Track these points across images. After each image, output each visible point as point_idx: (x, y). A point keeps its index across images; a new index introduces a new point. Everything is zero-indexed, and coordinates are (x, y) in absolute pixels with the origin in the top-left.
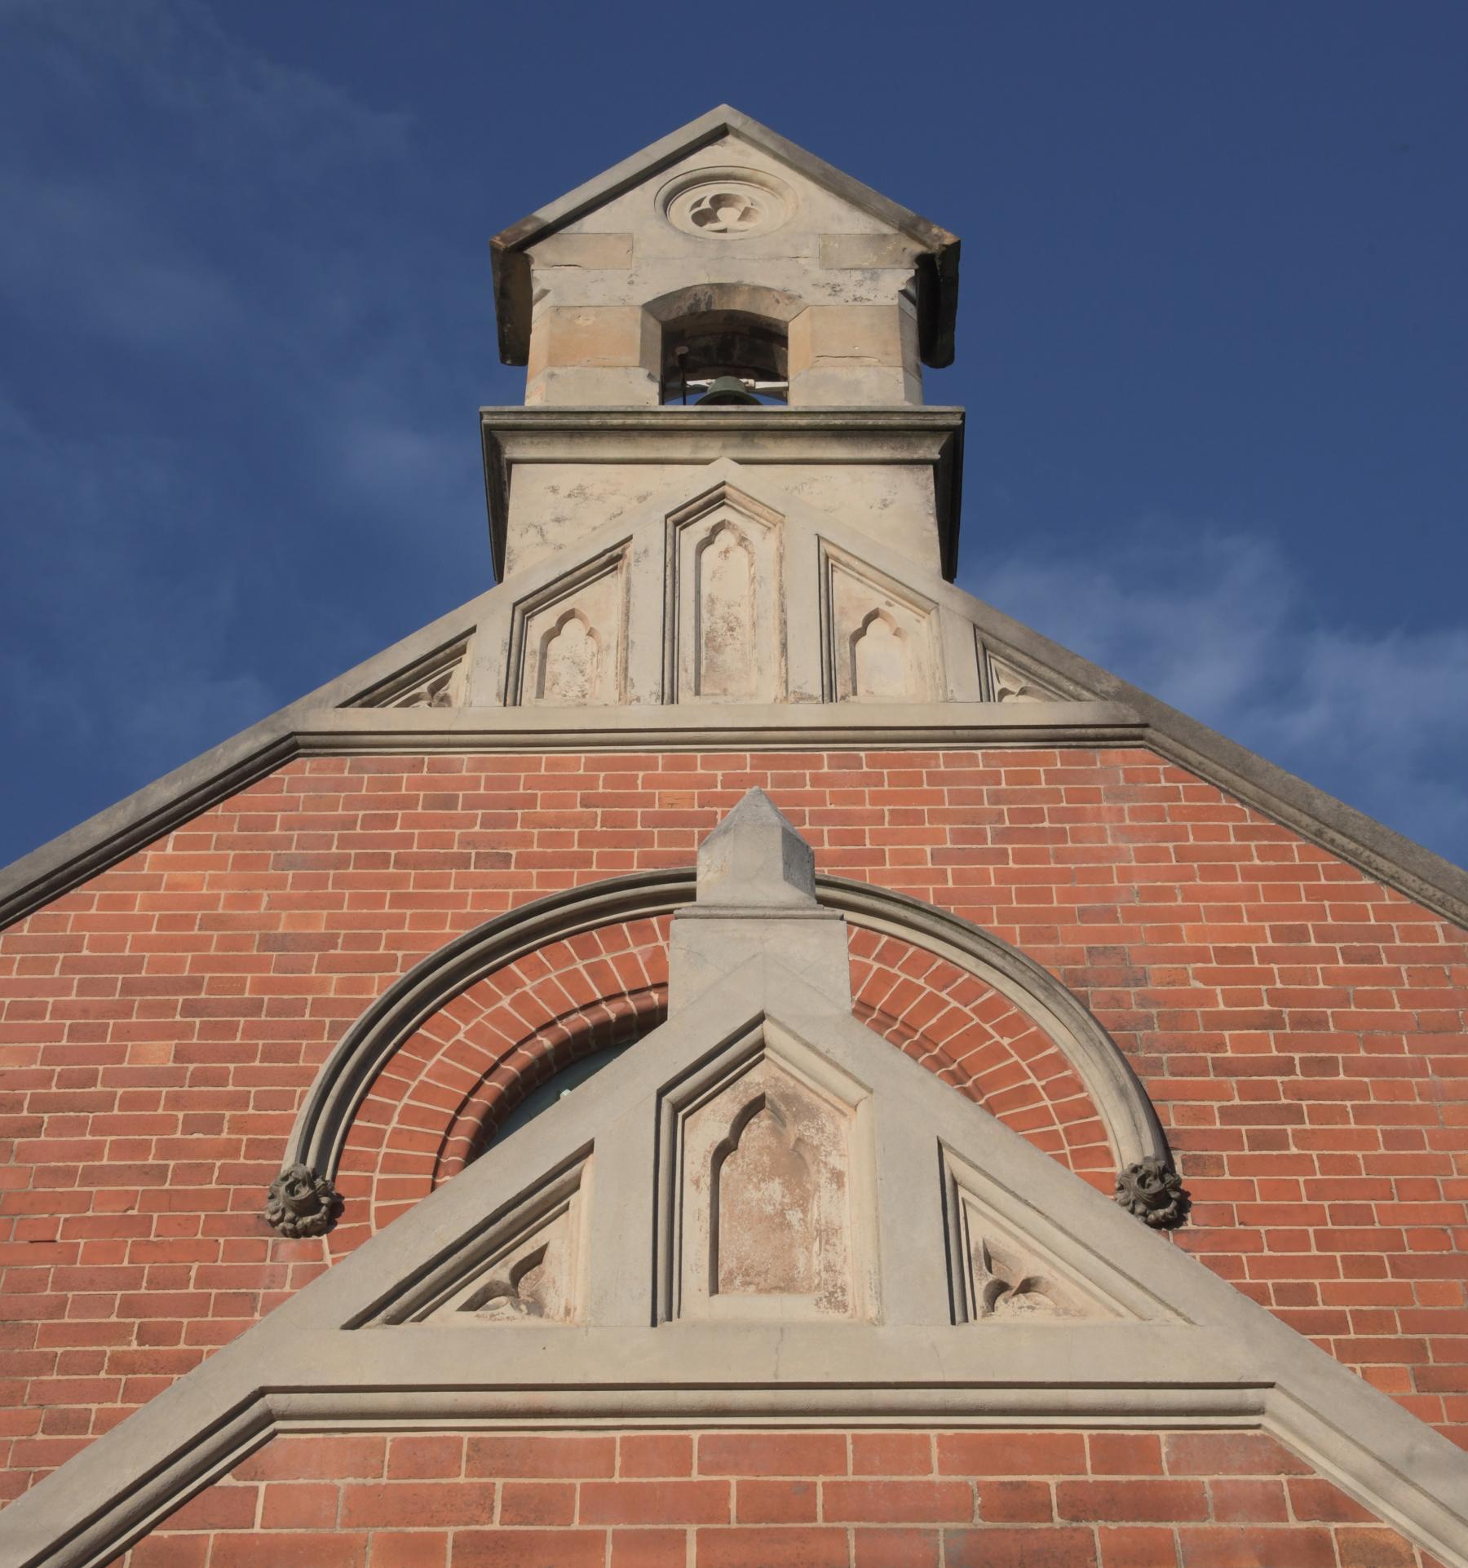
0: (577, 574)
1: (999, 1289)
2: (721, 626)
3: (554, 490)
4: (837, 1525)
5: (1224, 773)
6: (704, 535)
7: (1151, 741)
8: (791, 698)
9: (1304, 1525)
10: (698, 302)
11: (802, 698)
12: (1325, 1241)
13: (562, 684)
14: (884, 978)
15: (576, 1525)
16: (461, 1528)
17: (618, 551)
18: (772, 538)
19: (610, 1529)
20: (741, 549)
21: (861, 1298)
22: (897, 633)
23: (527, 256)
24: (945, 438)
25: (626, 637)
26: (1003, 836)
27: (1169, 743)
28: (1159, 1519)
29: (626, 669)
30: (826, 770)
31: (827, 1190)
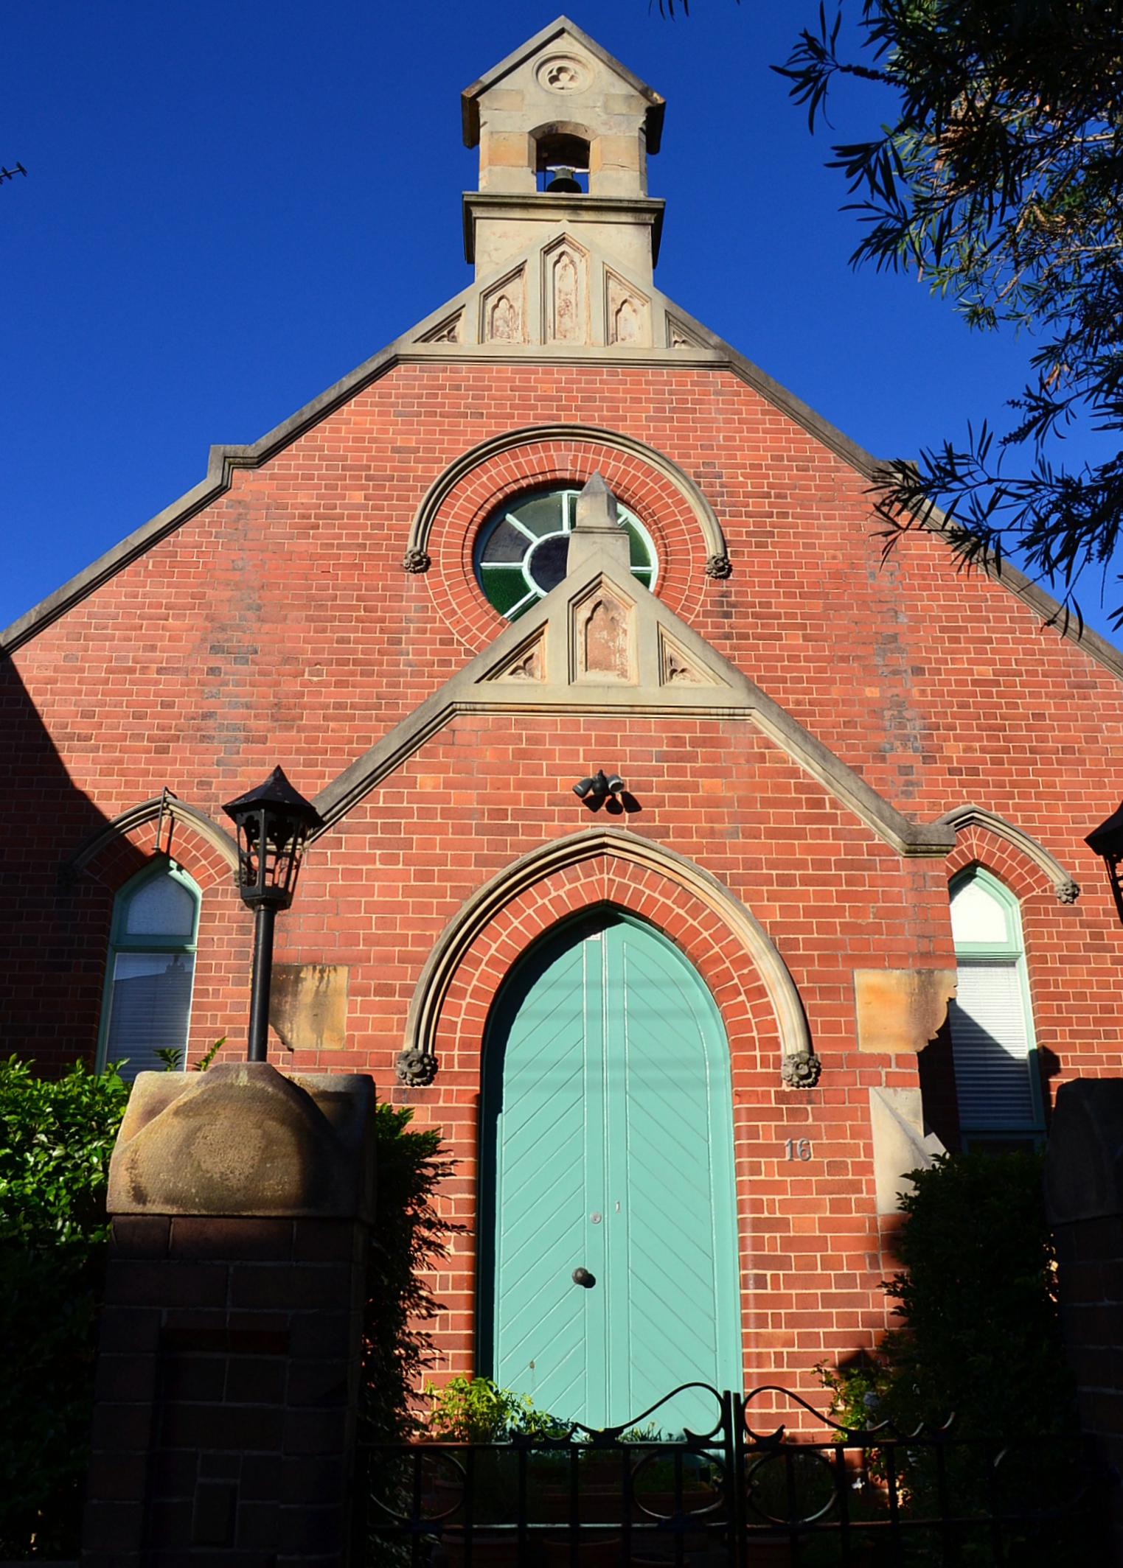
1: (674, 671)
12: (778, 585)
14: (626, 472)
21: (633, 677)
26: (673, 410)
31: (621, 636)
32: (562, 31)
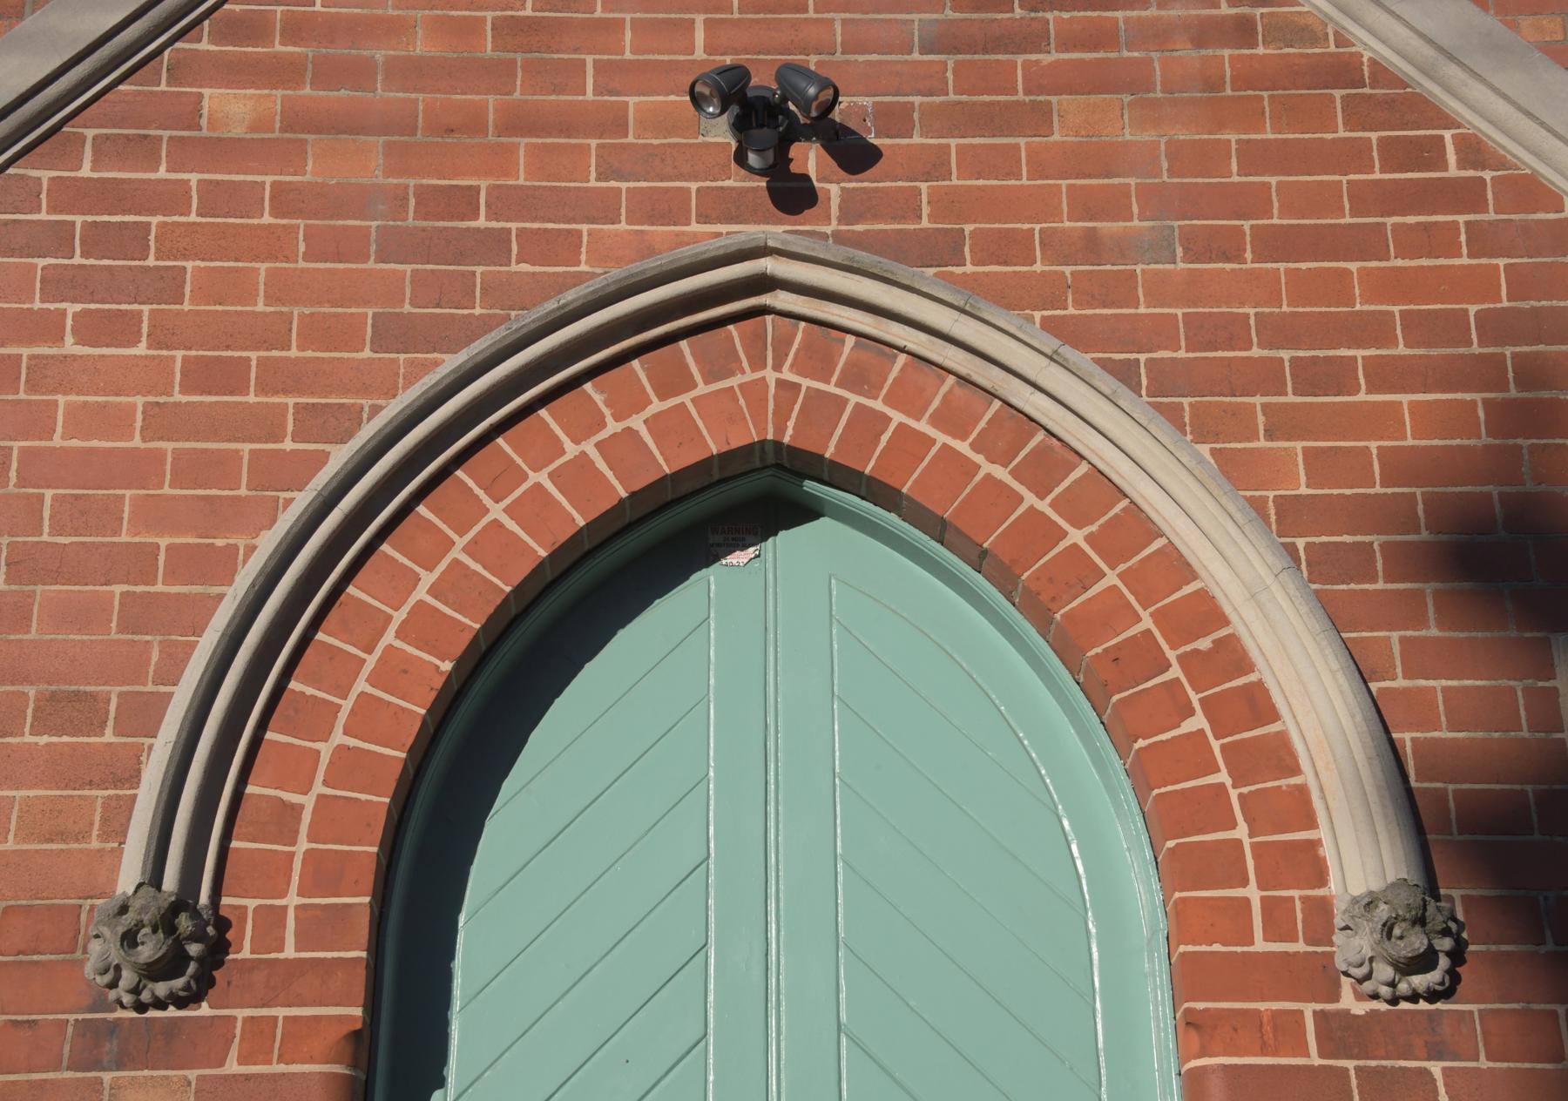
4: (825, 16)
9: (1234, 11)
15: (598, 13)
16: (499, 13)
19: (628, 17)
28: (1107, 9)
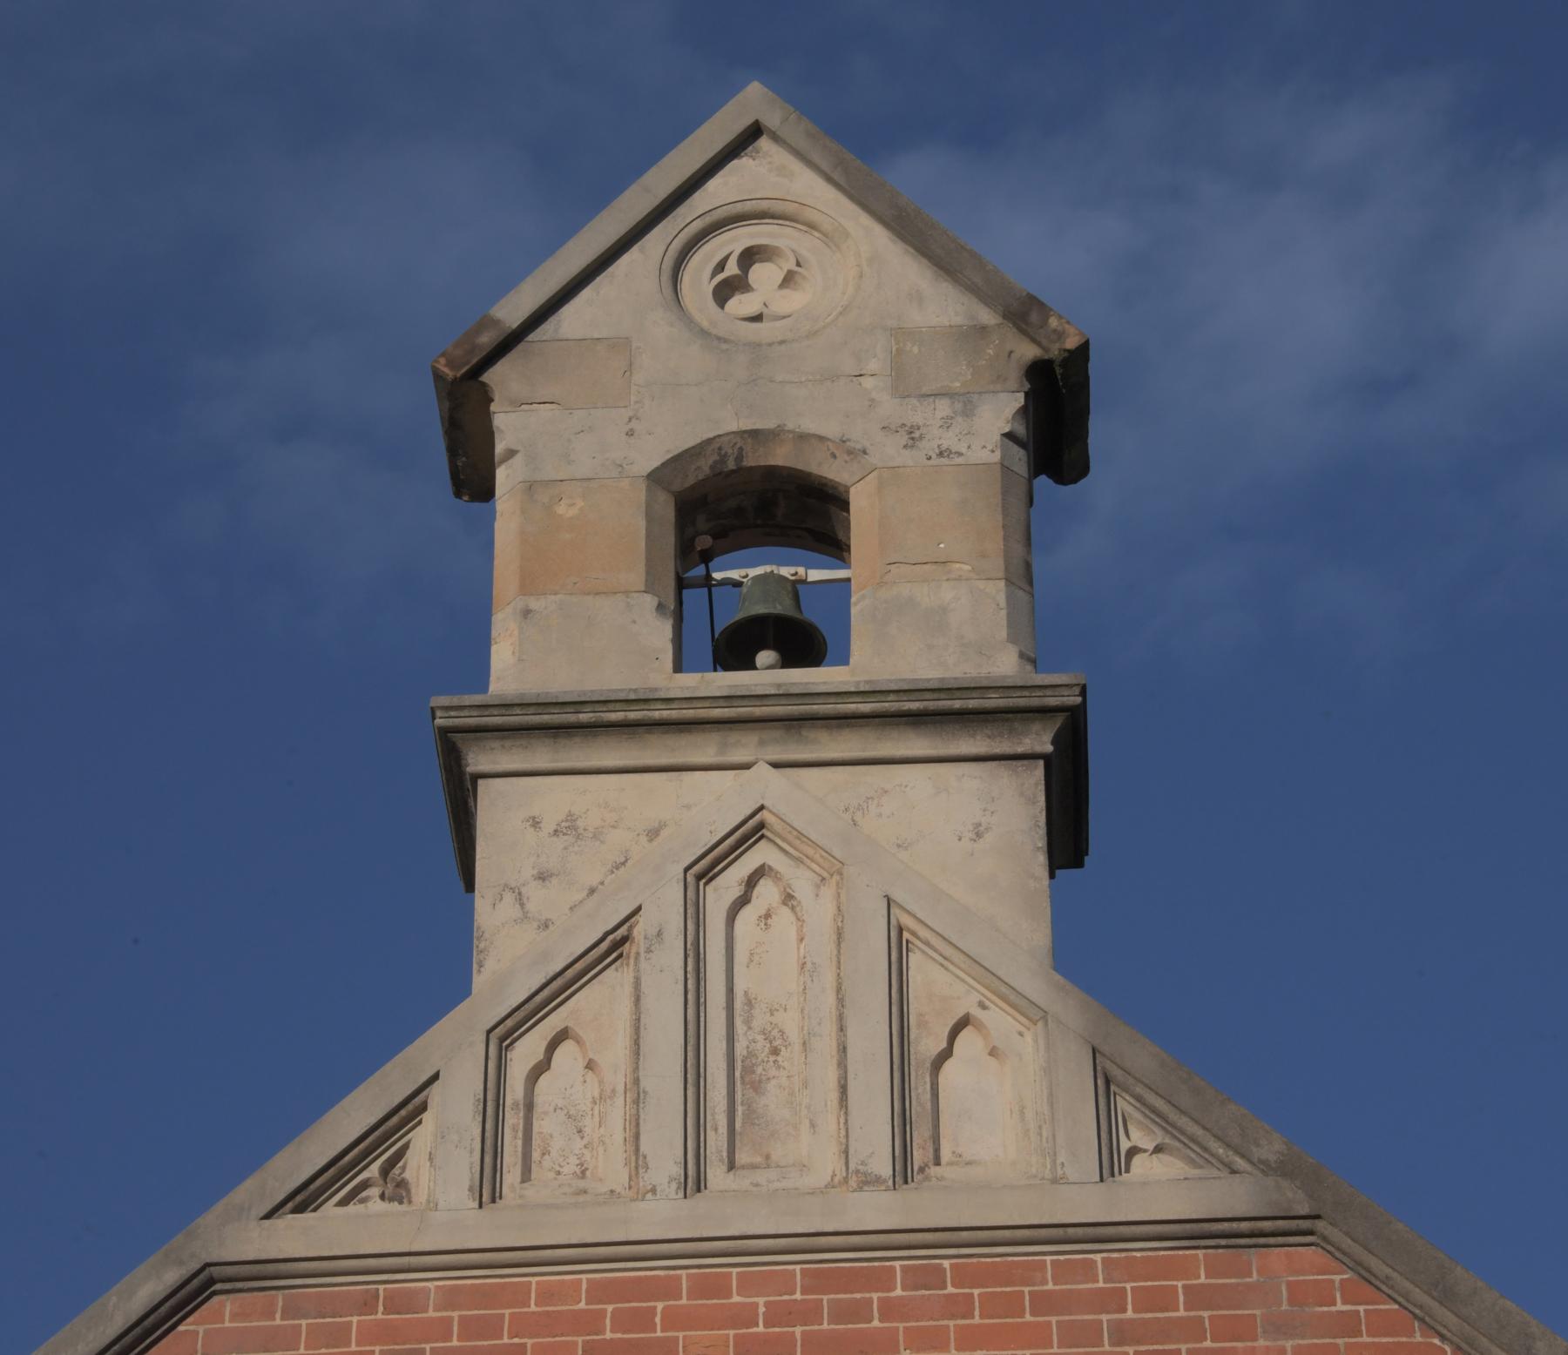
0: (570, 973)
2: (762, 1046)
3: (535, 823)
5: (1418, 1295)
6: (736, 892)
7: (1325, 1239)
8: (853, 1183)
10: (723, 458)
11: (868, 1181)
13: (554, 1153)
17: (622, 931)
18: (828, 892)
20: (785, 911)
22: (993, 1052)
23: (484, 385)
24: (1059, 721)
25: (637, 1081)
27: (1347, 1243)
29: (637, 1136)
30: (899, 1292)
32: (754, 132)
